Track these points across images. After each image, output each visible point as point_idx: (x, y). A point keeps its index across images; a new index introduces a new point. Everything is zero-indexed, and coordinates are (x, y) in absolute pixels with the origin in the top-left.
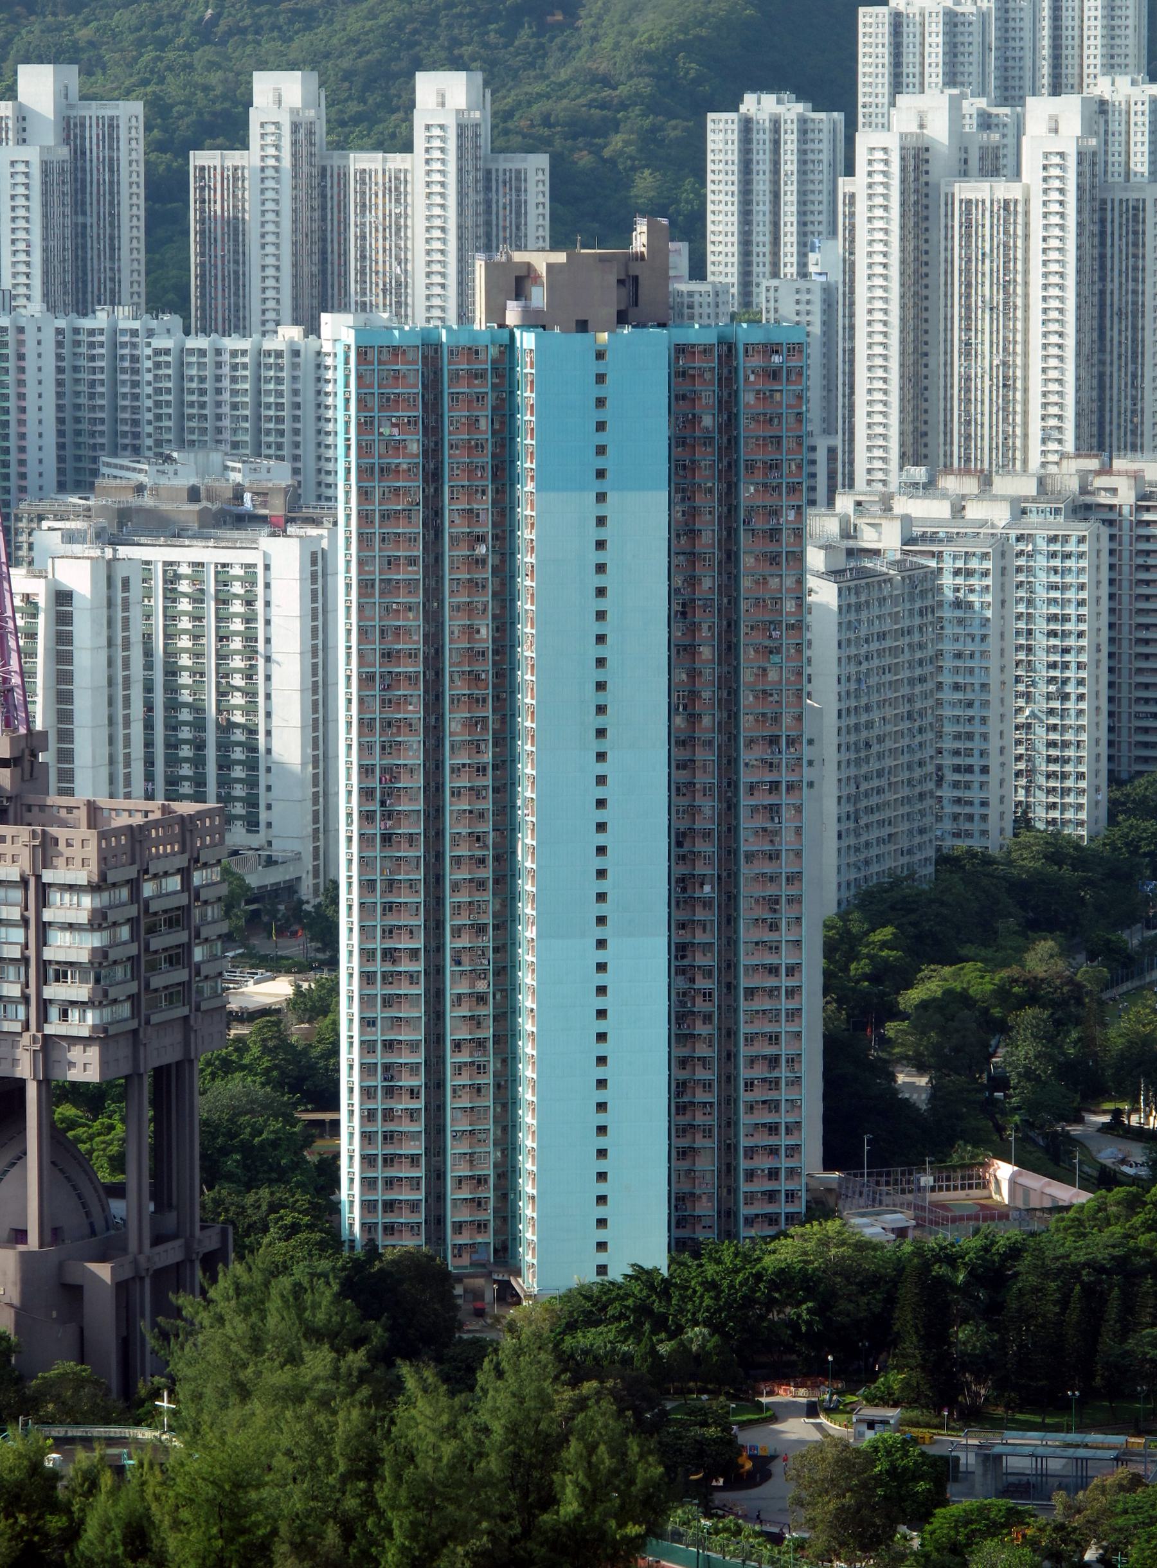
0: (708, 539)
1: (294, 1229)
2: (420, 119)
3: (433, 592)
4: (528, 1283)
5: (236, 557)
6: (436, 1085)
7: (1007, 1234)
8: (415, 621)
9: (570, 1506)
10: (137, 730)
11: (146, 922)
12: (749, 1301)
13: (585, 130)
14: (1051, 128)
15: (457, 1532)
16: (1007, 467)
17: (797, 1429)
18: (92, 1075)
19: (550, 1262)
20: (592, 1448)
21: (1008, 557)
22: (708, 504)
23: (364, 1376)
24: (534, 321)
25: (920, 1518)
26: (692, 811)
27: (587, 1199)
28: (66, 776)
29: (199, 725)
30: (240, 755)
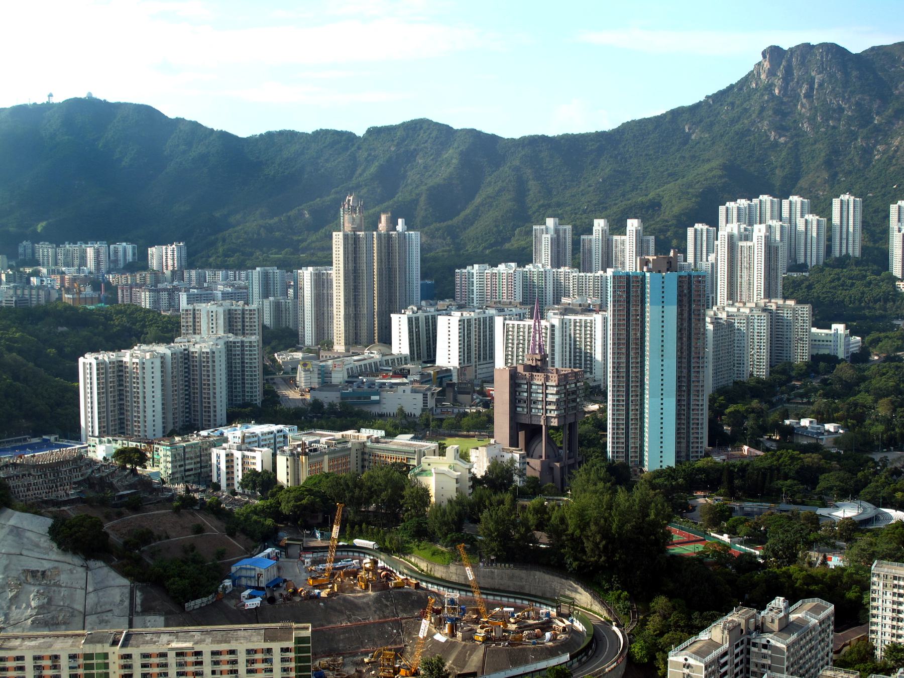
0: (686, 315)
1: (598, 457)
2: (628, 228)
3: (628, 326)
4: (646, 469)
5: (588, 318)
6: (627, 427)
7: (746, 461)
8: (624, 332)
9: (652, 517)
10: (568, 354)
11: (567, 393)
12: (692, 474)
13: (661, 231)
14: (759, 231)
15: (628, 521)
16: (749, 301)
17: (701, 501)
18: (556, 424)
19: (650, 464)
20: (657, 505)
21: (749, 320)
22: (686, 309)
23: (610, 488)
24: (649, 270)
25: (726, 520)
26: (682, 372)
27: (658, 452)
28: (553, 363)
29: (581, 352)
30: (589, 358)
